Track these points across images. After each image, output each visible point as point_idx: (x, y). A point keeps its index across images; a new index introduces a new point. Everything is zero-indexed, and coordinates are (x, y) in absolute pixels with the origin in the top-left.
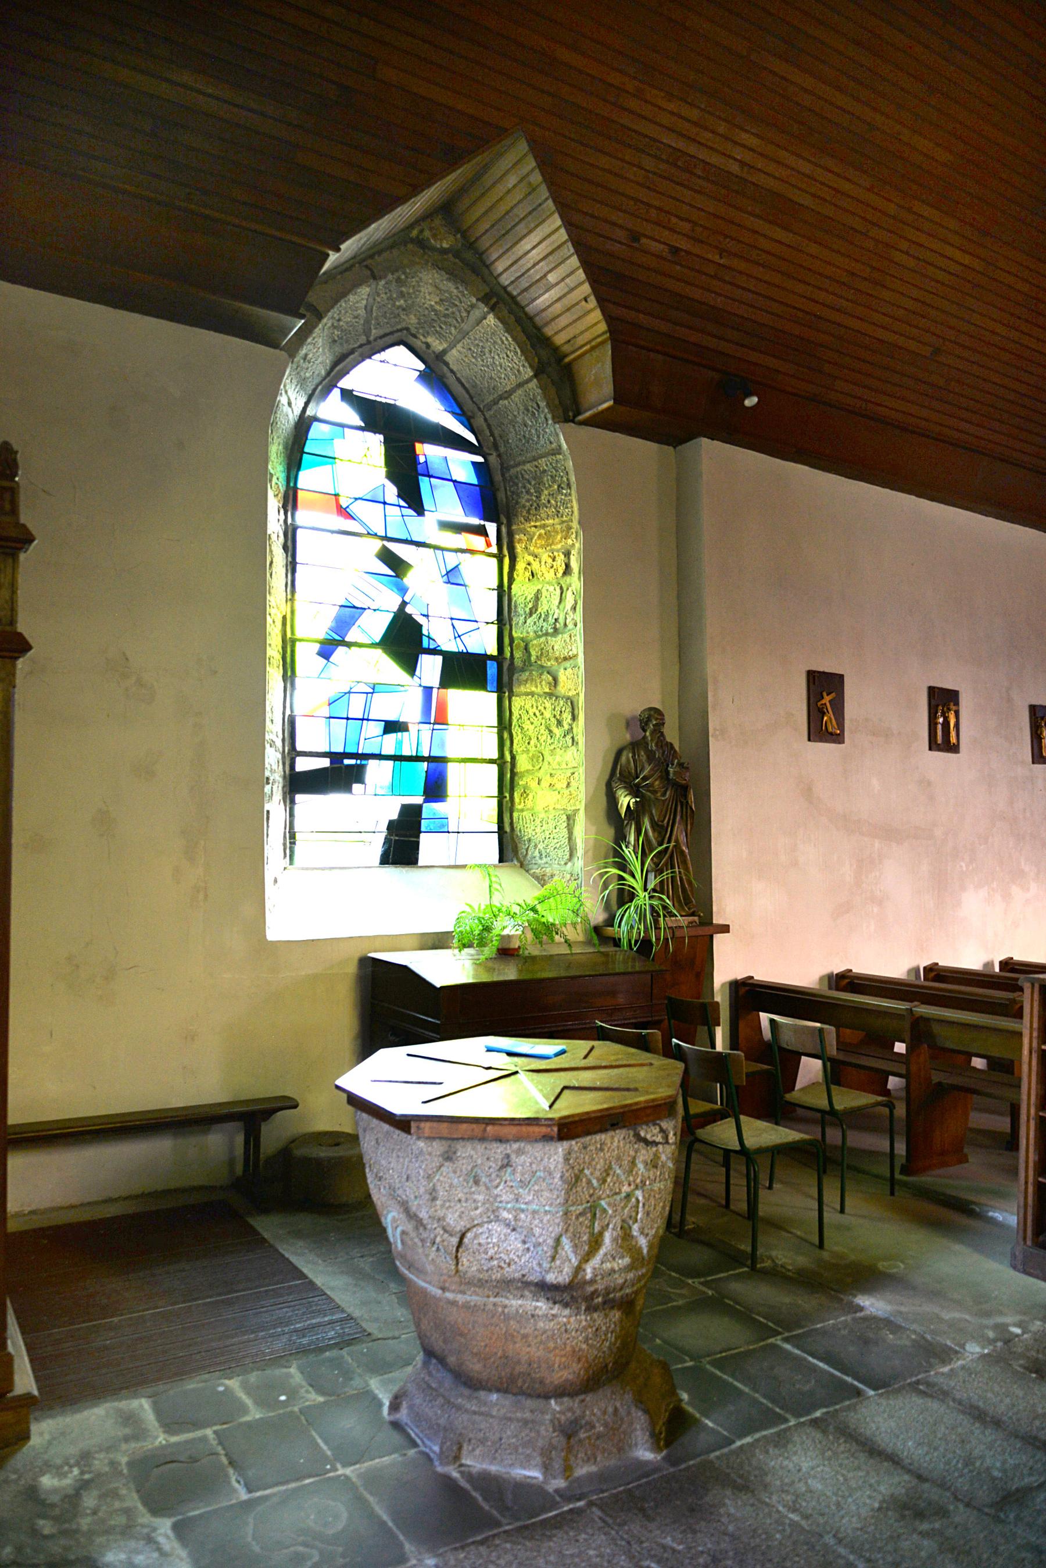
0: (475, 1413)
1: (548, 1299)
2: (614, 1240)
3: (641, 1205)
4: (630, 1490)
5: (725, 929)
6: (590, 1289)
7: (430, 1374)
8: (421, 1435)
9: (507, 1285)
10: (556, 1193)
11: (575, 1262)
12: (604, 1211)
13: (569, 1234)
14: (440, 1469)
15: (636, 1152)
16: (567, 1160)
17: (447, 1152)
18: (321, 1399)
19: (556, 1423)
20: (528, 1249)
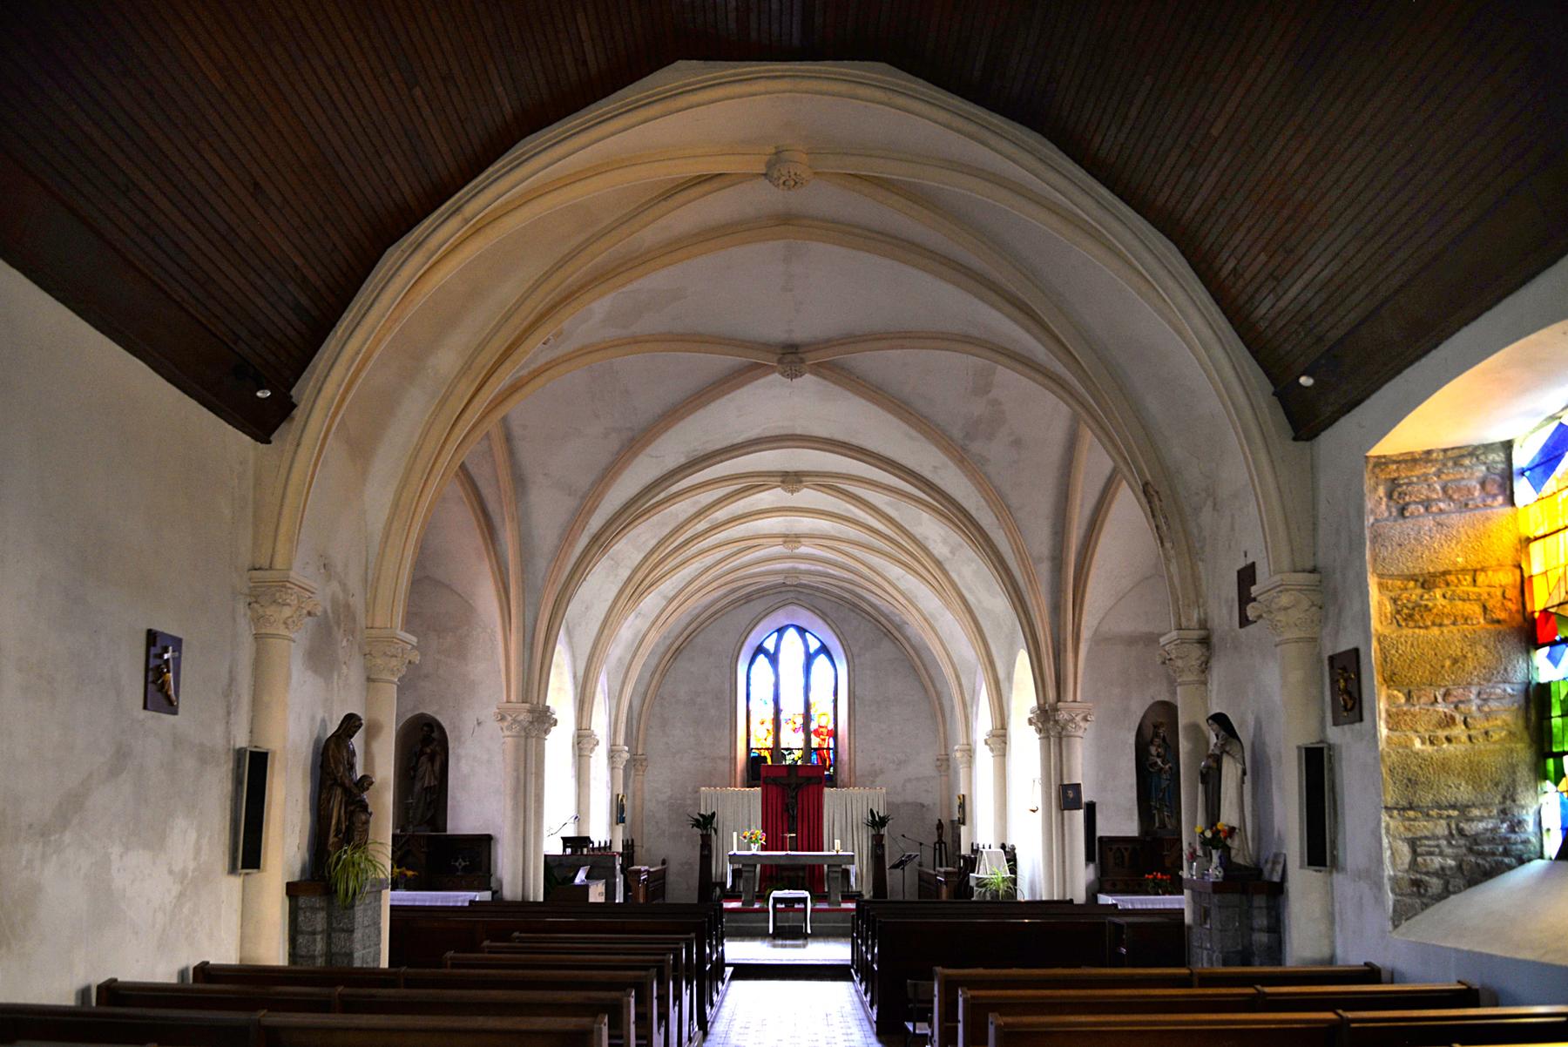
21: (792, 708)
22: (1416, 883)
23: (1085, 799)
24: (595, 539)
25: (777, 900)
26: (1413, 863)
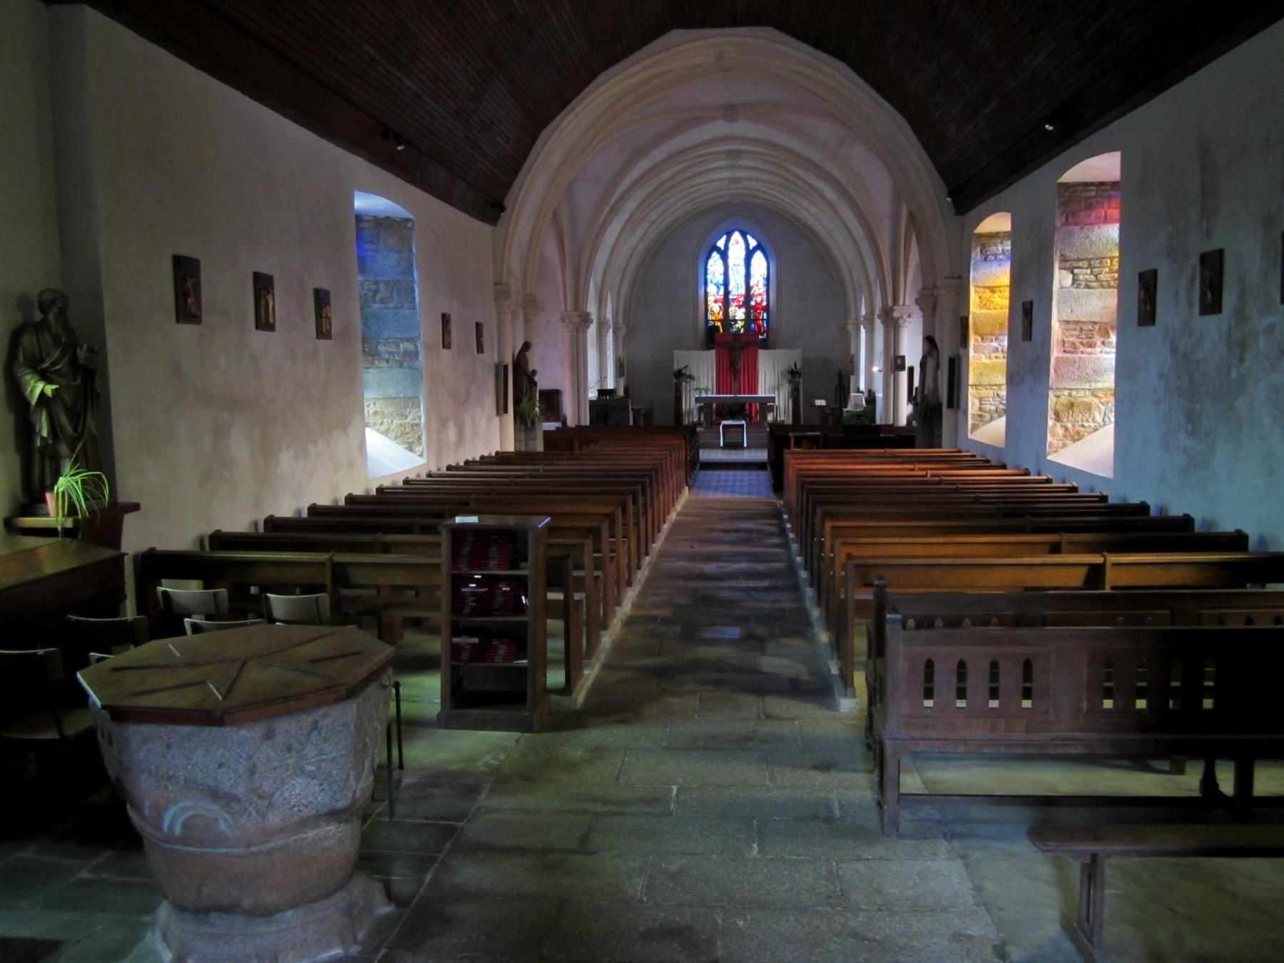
5: (135, 507)
9: (304, 824)
21: (737, 289)
22: (980, 416)
23: (908, 364)
24: (613, 207)
25: (725, 426)
26: (980, 409)
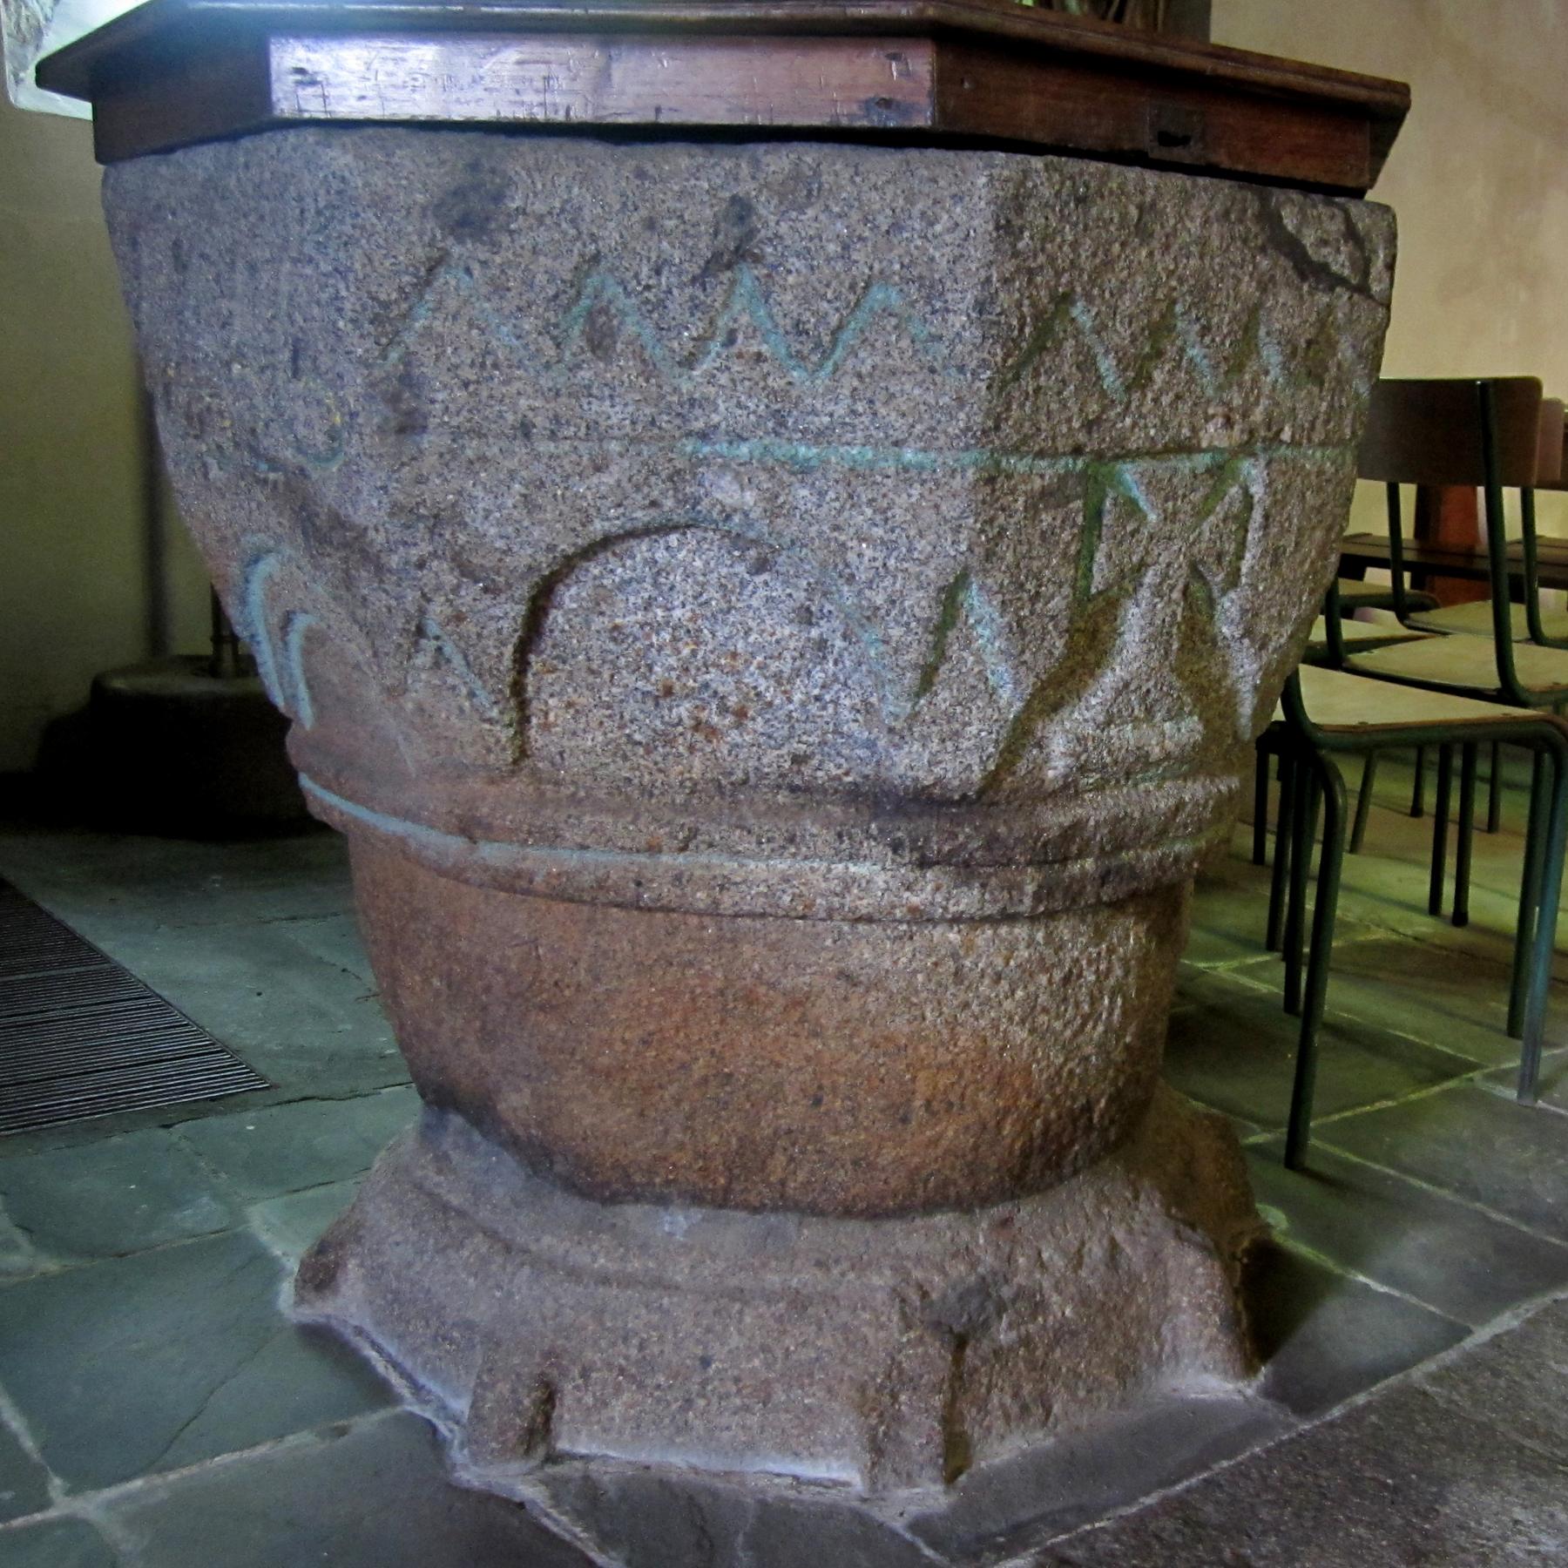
0: (604, 1280)
1: (896, 847)
2: (1157, 637)
3: (1257, 516)
4: (1181, 1502)
6: (1055, 819)
7: (442, 1160)
8: (408, 1364)
10: (953, 381)
11: (1010, 698)
12: (1131, 509)
13: (999, 577)
14: (471, 1474)
15: (1263, 289)
16: (1006, 229)
17: (459, 193)
18: (51, 1265)
19: (915, 1298)
20: (822, 645)
